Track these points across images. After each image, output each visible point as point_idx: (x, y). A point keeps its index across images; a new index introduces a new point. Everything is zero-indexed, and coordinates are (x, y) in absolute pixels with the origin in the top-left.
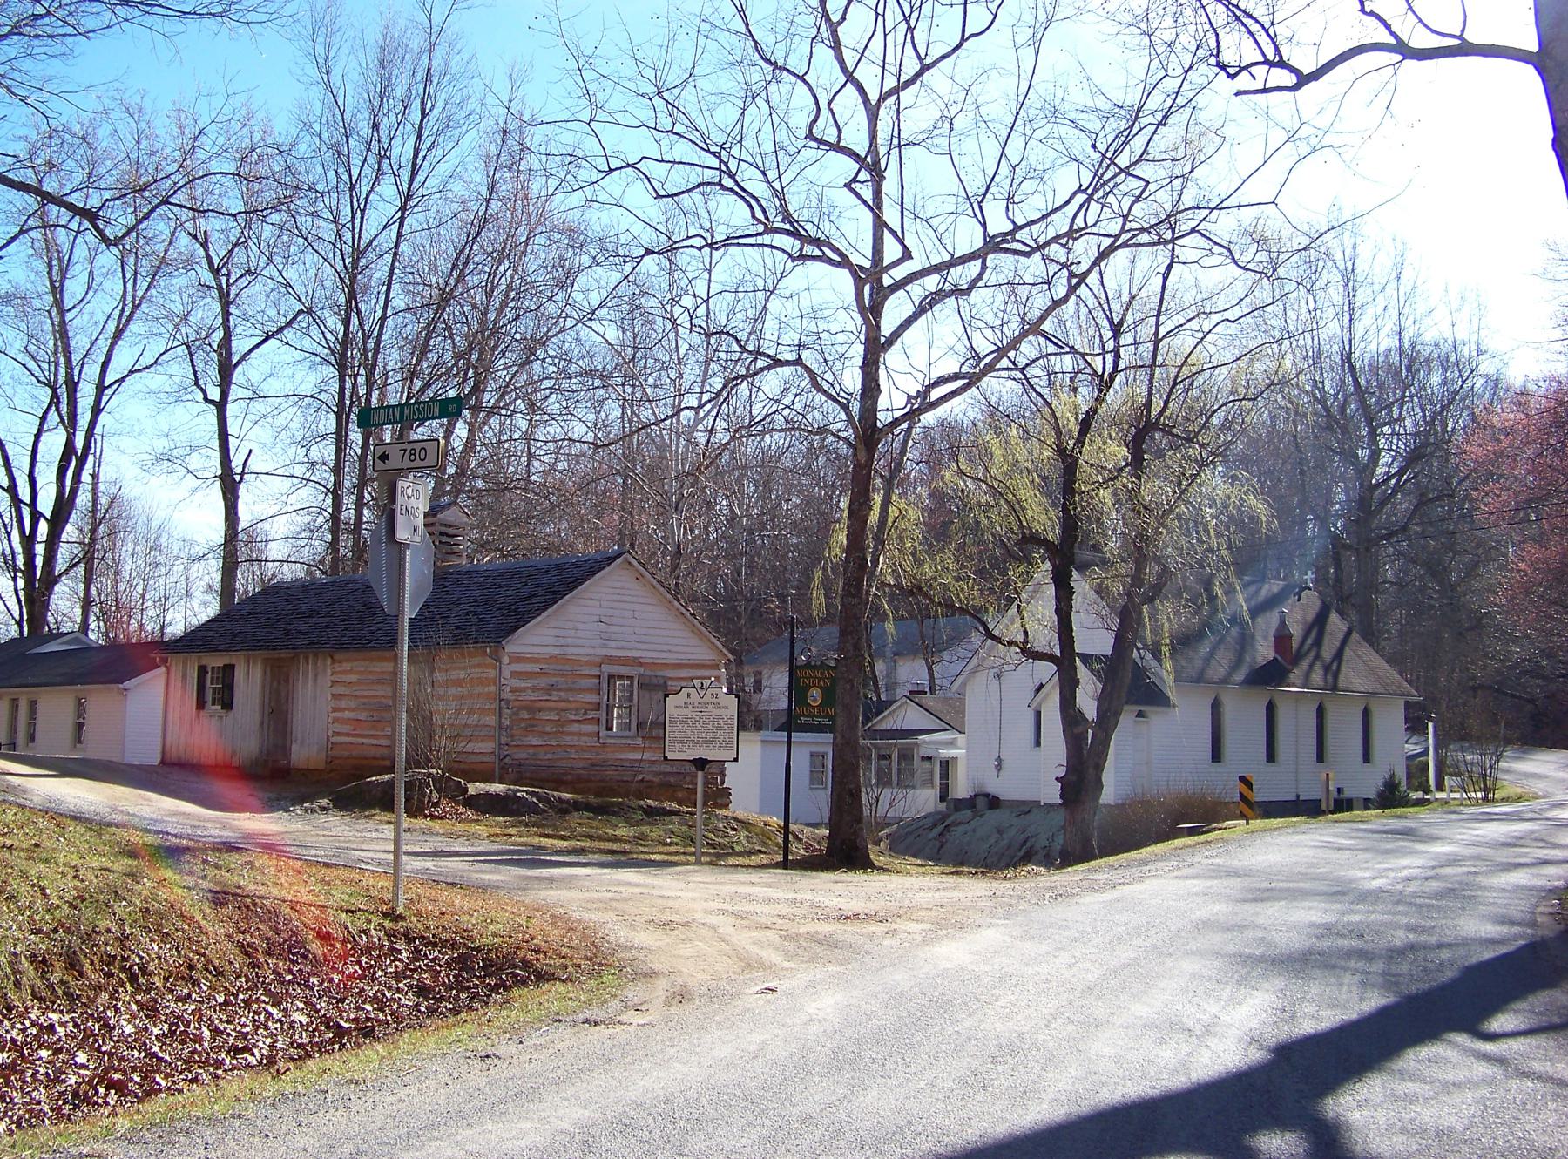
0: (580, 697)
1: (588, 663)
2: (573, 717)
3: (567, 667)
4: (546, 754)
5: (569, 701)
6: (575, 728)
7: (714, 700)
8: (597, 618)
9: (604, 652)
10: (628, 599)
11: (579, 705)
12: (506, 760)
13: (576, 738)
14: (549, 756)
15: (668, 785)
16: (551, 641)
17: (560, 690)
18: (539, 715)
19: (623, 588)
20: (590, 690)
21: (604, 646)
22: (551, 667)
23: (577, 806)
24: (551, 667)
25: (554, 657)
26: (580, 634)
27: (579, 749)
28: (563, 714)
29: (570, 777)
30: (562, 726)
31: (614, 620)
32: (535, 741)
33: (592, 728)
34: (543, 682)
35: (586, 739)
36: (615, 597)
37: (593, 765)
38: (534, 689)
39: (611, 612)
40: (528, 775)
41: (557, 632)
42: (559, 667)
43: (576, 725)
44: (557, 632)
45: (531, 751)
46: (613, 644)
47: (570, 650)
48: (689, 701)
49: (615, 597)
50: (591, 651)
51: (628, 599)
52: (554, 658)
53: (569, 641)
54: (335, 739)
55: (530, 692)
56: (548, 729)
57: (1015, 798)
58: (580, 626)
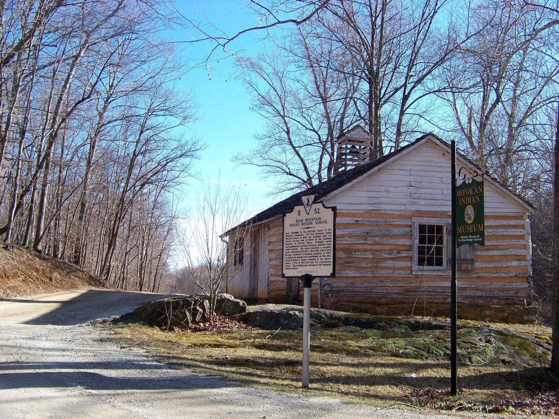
0: (393, 241)
1: (399, 216)
2: (386, 256)
3: (380, 220)
4: (362, 283)
5: (384, 245)
6: (390, 264)
7: (317, 216)
8: (408, 184)
9: (414, 208)
10: (435, 169)
11: (393, 247)
12: (326, 288)
13: (391, 271)
14: (366, 285)
15: (477, 306)
16: (365, 200)
17: (375, 236)
18: (354, 255)
19: (431, 161)
20: (403, 236)
21: (414, 204)
22: (366, 219)
23: (346, 322)
24: (366, 219)
25: (369, 212)
26: (390, 195)
27: (396, 279)
28: (378, 253)
29: (384, 300)
30: (378, 262)
31: (423, 185)
32: (352, 274)
33: (407, 264)
34: (359, 231)
35: (400, 272)
36: (422, 168)
37: (407, 291)
38: (350, 236)
39: (420, 179)
40: (345, 298)
41: (371, 194)
42: (373, 220)
43: (391, 262)
44: (371, 194)
45: (349, 281)
46: (423, 202)
47: (383, 207)
48: (299, 218)
49: (422, 168)
50: (403, 208)
51: (435, 169)
52: (369, 212)
53: (382, 200)
54: (272, 279)
55: (347, 238)
56: (364, 265)
57: (44, 388)
58: (391, 189)
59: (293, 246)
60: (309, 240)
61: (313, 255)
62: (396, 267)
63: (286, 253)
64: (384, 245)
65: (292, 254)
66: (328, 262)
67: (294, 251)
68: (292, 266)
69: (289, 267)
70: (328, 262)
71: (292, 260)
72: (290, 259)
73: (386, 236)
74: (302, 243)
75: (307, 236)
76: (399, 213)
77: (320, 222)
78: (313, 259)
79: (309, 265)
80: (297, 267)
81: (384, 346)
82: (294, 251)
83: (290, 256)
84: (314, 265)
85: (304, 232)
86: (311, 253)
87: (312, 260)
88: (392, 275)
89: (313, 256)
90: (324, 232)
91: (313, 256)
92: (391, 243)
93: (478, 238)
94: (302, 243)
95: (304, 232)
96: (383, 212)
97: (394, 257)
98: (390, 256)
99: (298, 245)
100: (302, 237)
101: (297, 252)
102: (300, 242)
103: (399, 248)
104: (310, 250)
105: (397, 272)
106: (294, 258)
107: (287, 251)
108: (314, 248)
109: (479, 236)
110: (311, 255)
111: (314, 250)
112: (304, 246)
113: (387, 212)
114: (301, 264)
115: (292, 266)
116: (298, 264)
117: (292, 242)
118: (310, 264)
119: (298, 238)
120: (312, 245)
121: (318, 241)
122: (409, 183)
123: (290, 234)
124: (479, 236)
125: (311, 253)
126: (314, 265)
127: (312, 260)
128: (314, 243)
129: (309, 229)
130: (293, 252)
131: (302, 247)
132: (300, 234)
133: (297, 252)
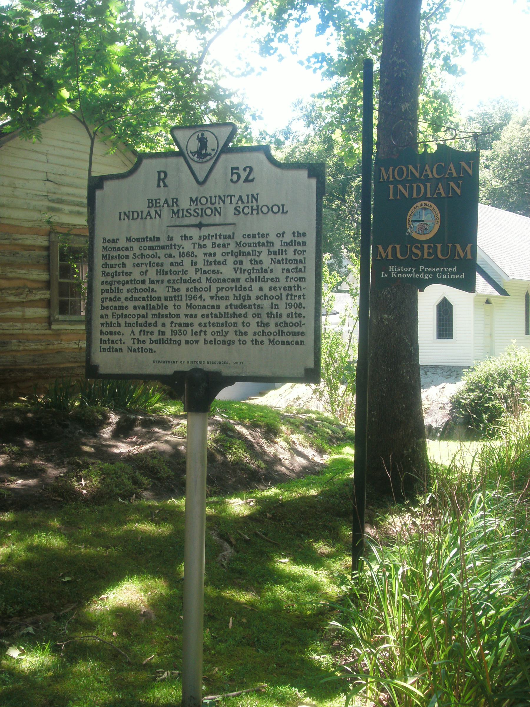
0: (22, 273)
2: (12, 298)
13: (19, 325)
31: (67, 180)
50: (36, 216)
59: (134, 281)
60: (207, 263)
61: (223, 310)
62: (26, 317)
63: (103, 300)
64: (8, 279)
65: (131, 304)
66: (293, 334)
67: (137, 295)
68: (129, 343)
69: (117, 346)
70: (293, 334)
71: (130, 325)
72: (122, 321)
73: (11, 264)
74: (177, 273)
75: (199, 253)
76: (30, 224)
77: (258, 210)
78: (226, 324)
79: (187, 342)
80: (154, 346)
81: (491, 582)
82: (137, 295)
83: (119, 312)
84: (230, 343)
85: (185, 238)
86: (215, 303)
87: (218, 324)
88: (21, 332)
89: (226, 315)
90: (272, 238)
91: (226, 315)
92: (21, 276)
93: (455, 274)
94: (177, 273)
95: (185, 238)
96: (6, 222)
97: (24, 300)
98: (16, 299)
99: (154, 277)
100: (175, 252)
101: (151, 298)
102: (167, 268)
103: (29, 284)
104: (213, 293)
105: (28, 326)
106: (138, 316)
107: (106, 295)
108: (228, 289)
109: (455, 269)
110: (215, 311)
111: (230, 294)
112: (185, 282)
113: (13, 223)
114: (168, 336)
115: (129, 343)
116: (155, 337)
117: (129, 268)
118: (209, 337)
119: (156, 256)
120: (219, 280)
121: (247, 265)
122: (45, 174)
123: (122, 243)
124: (455, 269)
125: (215, 303)
126: (230, 343)
127: (218, 324)
128: (227, 271)
129: (205, 231)
130: (132, 299)
131: (176, 286)
132: (163, 243)
133: (151, 298)
